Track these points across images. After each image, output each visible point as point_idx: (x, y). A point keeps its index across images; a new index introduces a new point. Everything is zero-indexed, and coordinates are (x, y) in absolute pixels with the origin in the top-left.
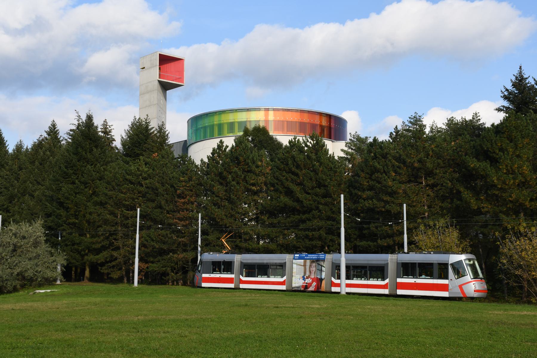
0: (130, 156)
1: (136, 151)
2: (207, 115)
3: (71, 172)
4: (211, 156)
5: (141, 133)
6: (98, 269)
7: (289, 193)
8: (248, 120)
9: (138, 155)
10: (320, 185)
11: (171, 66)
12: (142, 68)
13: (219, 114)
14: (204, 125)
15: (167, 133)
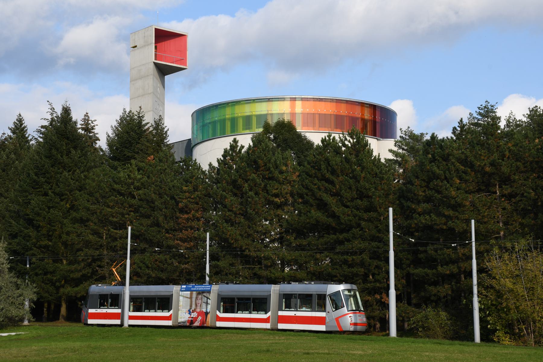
0: (119, 160)
1: (126, 153)
2: (216, 107)
3: (43, 180)
4: (222, 158)
6: (78, 304)
7: (322, 206)
8: (270, 112)
9: (128, 158)
10: (362, 196)
11: (171, 44)
13: (232, 106)
14: (213, 120)
15: (165, 130)
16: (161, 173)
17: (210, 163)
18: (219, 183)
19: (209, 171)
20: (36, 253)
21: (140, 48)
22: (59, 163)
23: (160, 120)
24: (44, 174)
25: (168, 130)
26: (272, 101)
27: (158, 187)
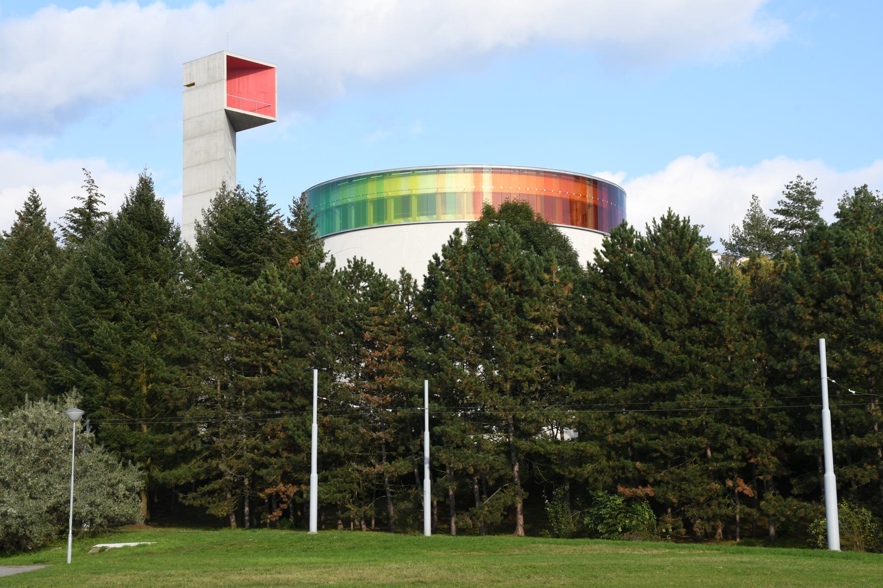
2: (350, 181)
3: (114, 294)
6: (177, 497)
7: (624, 336)
8: (440, 191)
10: (696, 320)
11: (249, 81)
13: (378, 179)
14: (345, 202)
20: (104, 414)
22: (139, 268)
24: (116, 285)
26: (445, 173)
27: (322, 307)
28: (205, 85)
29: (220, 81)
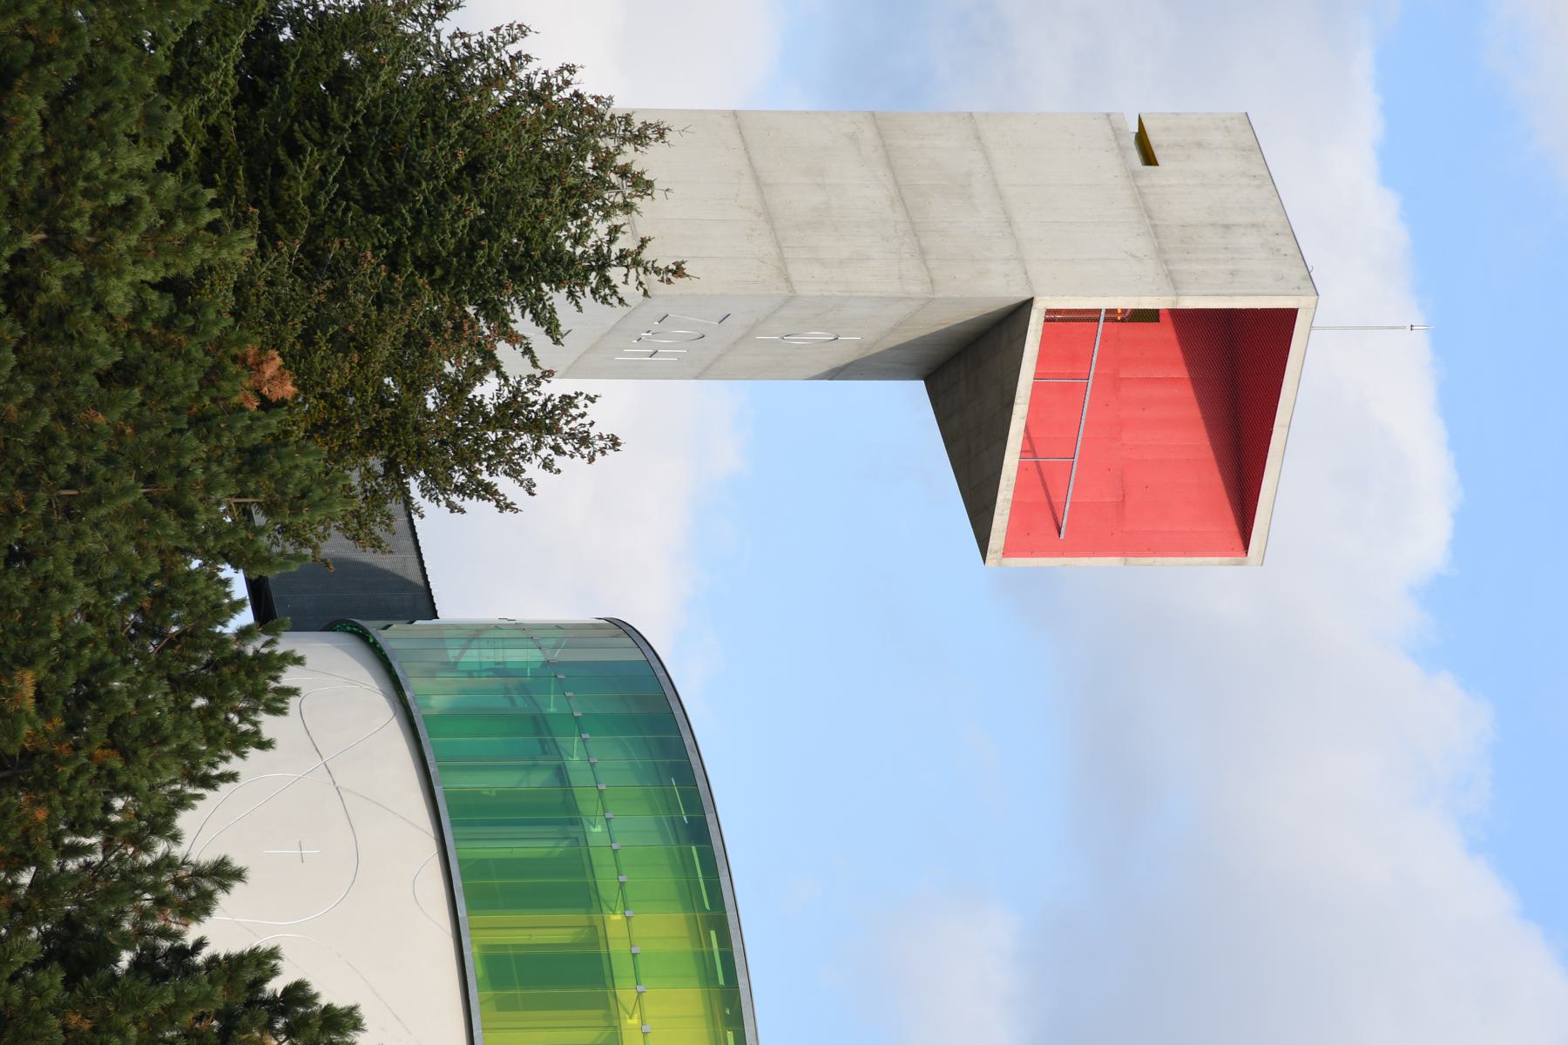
0: (250, 96)
1: (313, 158)
4: (275, 986)
5: (501, 206)
9: (266, 177)
11: (1176, 430)
12: (1142, 140)
13: (704, 960)
15: (505, 485)
16: (150, 479)
17: (238, 875)
18: (69, 983)
19: (168, 862)
21: (1139, 194)
23: (585, 440)
25: (504, 506)
28: (1148, 213)
29: (1170, 275)
